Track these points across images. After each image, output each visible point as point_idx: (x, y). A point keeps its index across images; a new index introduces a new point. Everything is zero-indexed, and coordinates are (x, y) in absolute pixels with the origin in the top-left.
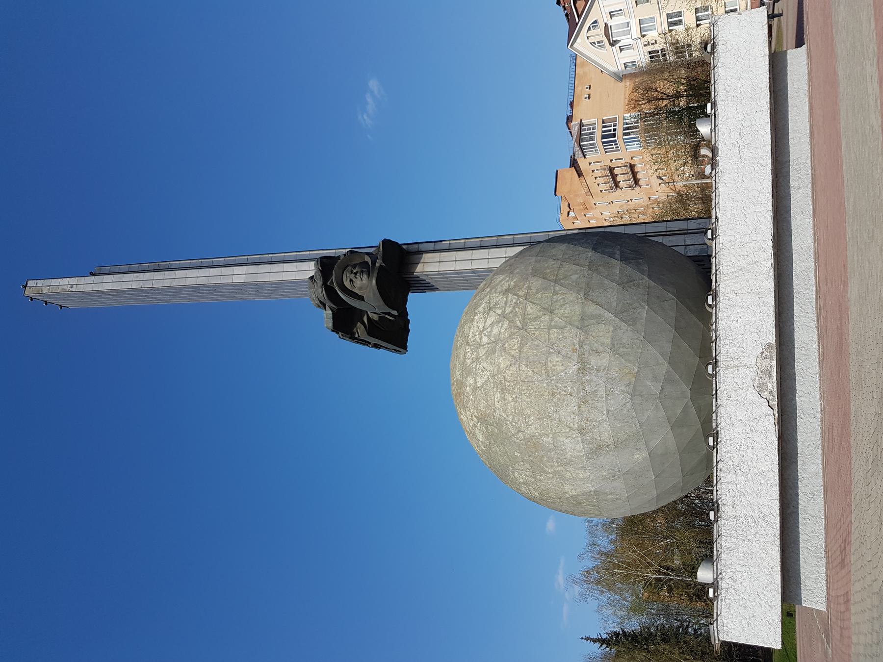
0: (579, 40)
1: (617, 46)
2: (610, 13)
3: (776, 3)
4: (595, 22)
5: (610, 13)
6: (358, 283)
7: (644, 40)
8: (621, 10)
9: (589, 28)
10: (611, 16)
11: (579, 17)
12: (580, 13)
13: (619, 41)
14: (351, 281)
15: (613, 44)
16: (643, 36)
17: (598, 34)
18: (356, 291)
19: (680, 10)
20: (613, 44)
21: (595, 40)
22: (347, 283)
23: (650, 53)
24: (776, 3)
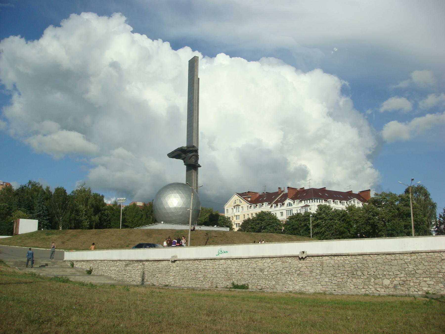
0: (237, 196)
1: (234, 208)
2: (283, 212)
3: (304, 258)
4: (241, 202)
5: (283, 212)
6: (193, 159)
7: (234, 216)
8: (283, 215)
9: (240, 200)
10: (242, 207)
11: (243, 198)
12: (245, 198)
13: (235, 209)
14: (194, 158)
15: (234, 207)
16: (235, 216)
17: (238, 203)
18: (191, 158)
19: (123, 229)
20: (234, 207)
21: (237, 202)
22: (193, 157)
23: (230, 218)
24: (304, 258)
